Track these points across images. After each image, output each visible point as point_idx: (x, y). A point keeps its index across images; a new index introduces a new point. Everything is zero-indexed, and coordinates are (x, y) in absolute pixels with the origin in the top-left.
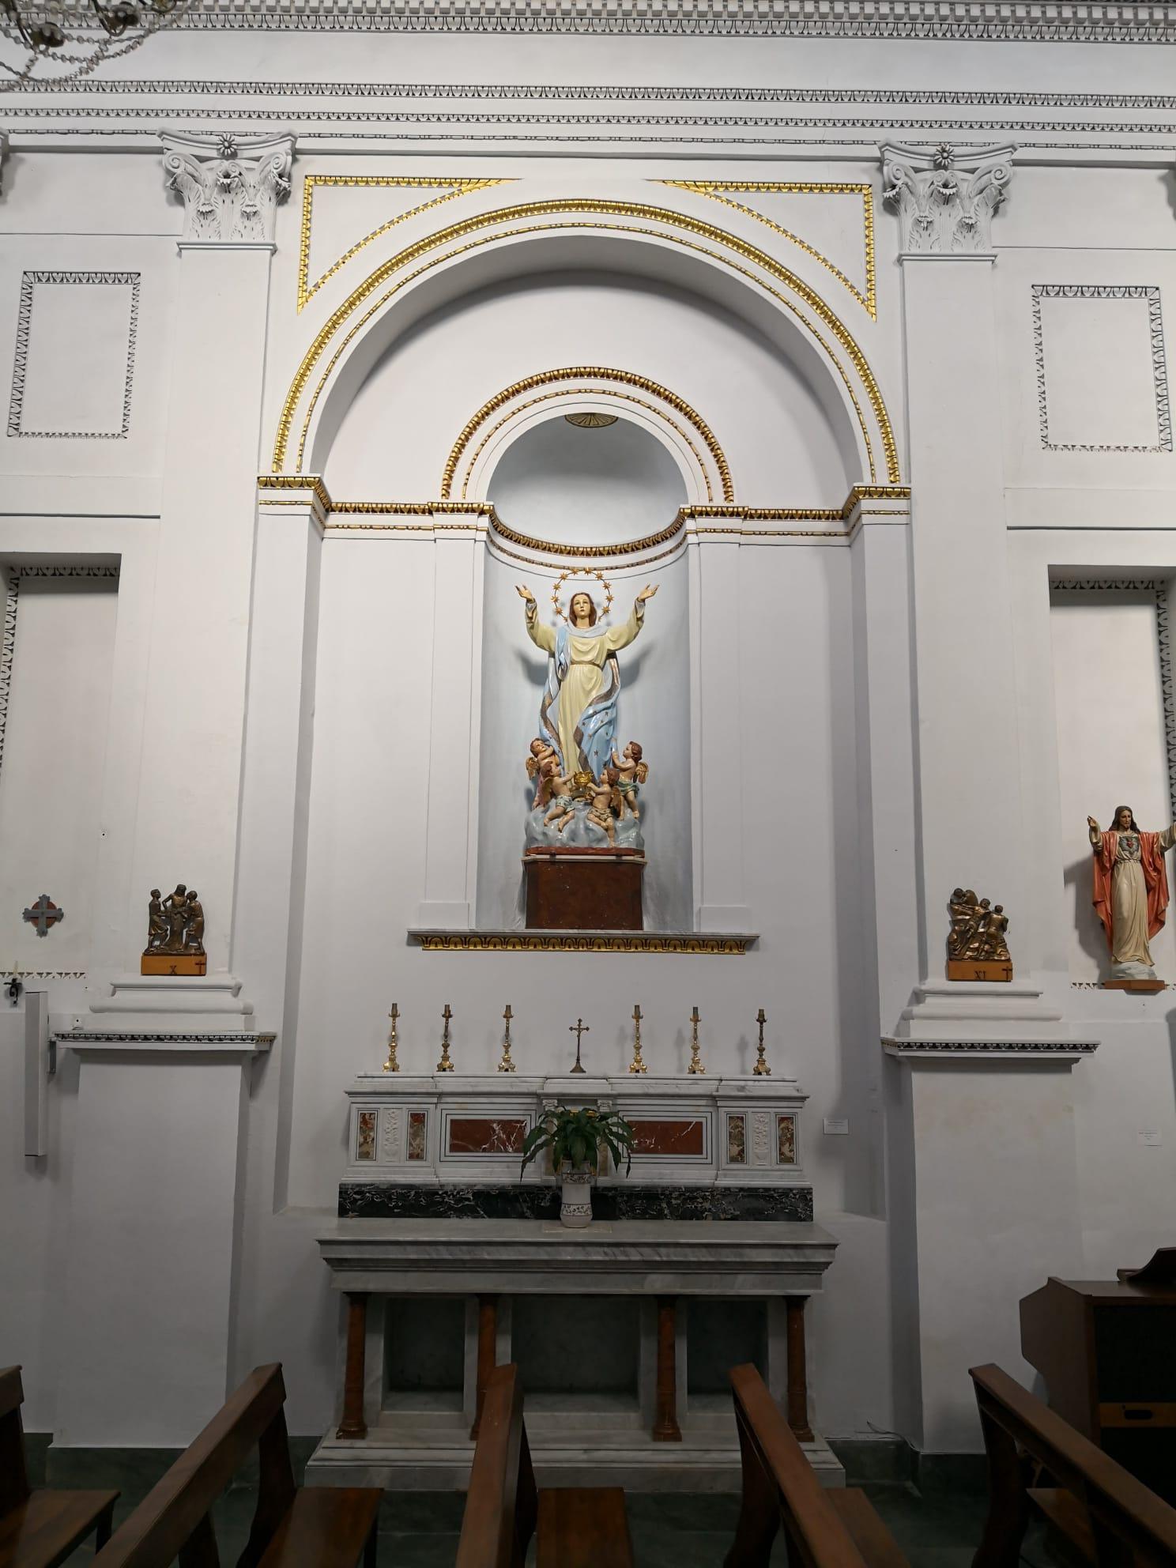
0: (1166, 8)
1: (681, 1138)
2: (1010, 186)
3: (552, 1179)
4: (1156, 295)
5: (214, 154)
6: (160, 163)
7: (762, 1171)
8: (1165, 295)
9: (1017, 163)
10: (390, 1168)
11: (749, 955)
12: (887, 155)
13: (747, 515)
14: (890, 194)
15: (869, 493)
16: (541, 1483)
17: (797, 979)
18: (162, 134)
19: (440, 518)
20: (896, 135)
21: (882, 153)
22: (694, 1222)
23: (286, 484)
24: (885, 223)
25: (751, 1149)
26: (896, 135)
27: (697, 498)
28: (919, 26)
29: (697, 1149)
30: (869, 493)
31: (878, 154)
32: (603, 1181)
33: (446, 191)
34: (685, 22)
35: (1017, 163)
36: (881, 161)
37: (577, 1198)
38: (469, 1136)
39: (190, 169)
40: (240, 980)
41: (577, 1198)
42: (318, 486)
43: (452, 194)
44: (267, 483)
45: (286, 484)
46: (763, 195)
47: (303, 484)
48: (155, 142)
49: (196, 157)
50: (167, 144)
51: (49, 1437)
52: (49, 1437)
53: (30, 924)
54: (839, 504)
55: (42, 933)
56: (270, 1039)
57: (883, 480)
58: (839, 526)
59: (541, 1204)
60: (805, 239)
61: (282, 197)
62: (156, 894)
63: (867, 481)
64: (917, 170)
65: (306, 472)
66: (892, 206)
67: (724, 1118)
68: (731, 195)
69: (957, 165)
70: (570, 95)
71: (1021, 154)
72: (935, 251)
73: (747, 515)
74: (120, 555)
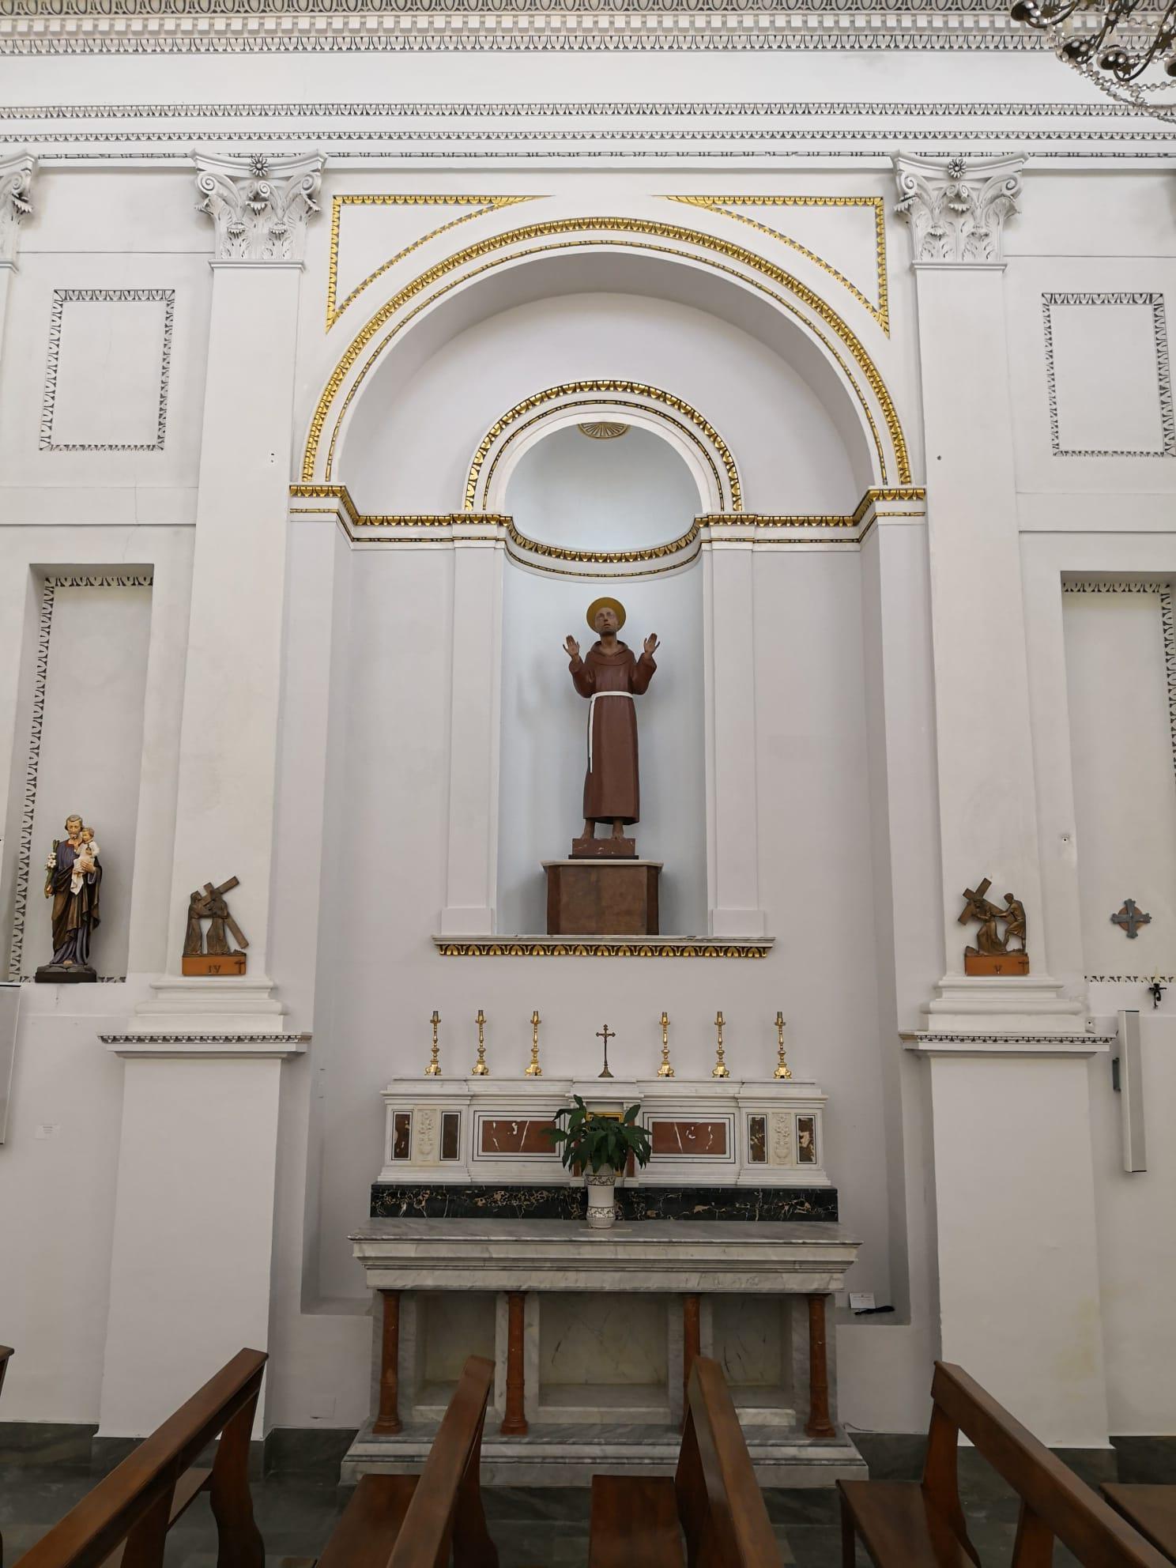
0: (245, 18)
1: (704, 1138)
2: (1021, 196)
3: (577, 1182)
4: (1160, 301)
5: (246, 174)
6: (193, 183)
7: (783, 1172)
8: (1167, 301)
9: (1027, 173)
10: (425, 1168)
11: (770, 958)
12: (901, 166)
13: (755, 521)
14: (902, 206)
15: (882, 495)
16: (484, 1480)
17: (809, 979)
18: (194, 155)
19: (458, 530)
20: (907, 147)
21: (894, 164)
22: (562, 1221)
23: (315, 492)
24: (895, 235)
25: (771, 1147)
26: (907, 147)
27: (709, 506)
28: (447, 39)
29: (719, 1147)
30: (882, 495)
31: (891, 166)
32: (631, 1183)
33: (473, 209)
34: (917, 38)
35: (1027, 173)
36: (894, 172)
37: (601, 1201)
38: (502, 1137)
39: (226, 193)
40: (278, 982)
41: (601, 1201)
42: (343, 494)
43: (480, 212)
44: (296, 492)
45: (315, 492)
46: (769, 208)
47: (330, 492)
48: (189, 163)
49: (230, 177)
50: (201, 165)
51: (95, 1428)
52: (95, 1428)
53: (1121, 906)
54: (848, 511)
55: (1146, 919)
56: (306, 1038)
57: (894, 483)
58: (851, 532)
59: (561, 1205)
60: (826, 250)
61: (313, 215)
62: (986, 883)
63: (878, 485)
64: (234, 179)
65: (335, 481)
66: (902, 217)
67: (744, 1117)
68: (746, 211)
69: (968, 176)
70: (328, 112)
71: (1032, 163)
72: (948, 260)
73: (755, 521)
74: (31, 565)
